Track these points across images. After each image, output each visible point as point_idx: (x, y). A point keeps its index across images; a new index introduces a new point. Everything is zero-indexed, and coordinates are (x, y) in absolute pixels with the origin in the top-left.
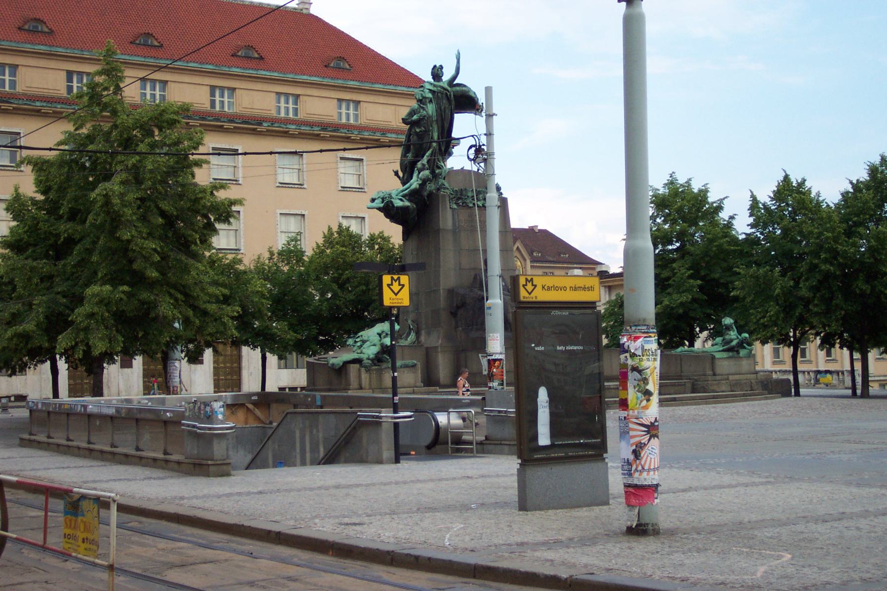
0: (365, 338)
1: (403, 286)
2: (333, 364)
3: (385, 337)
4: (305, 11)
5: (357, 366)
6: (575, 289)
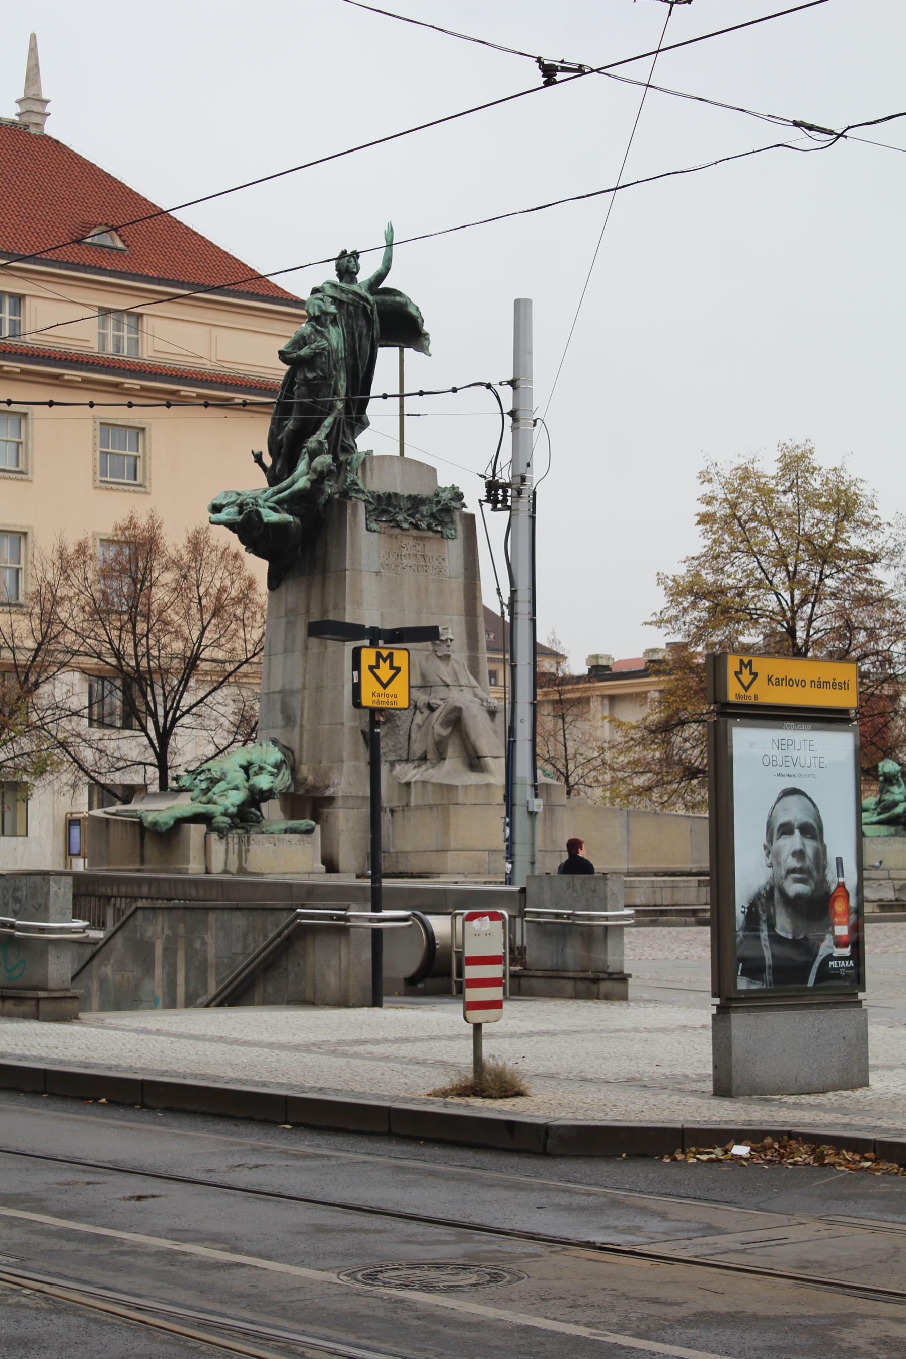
0: (216, 774)
1: (398, 670)
2: (155, 824)
3: (256, 774)
4: (33, 130)
5: (203, 828)
6: (820, 684)
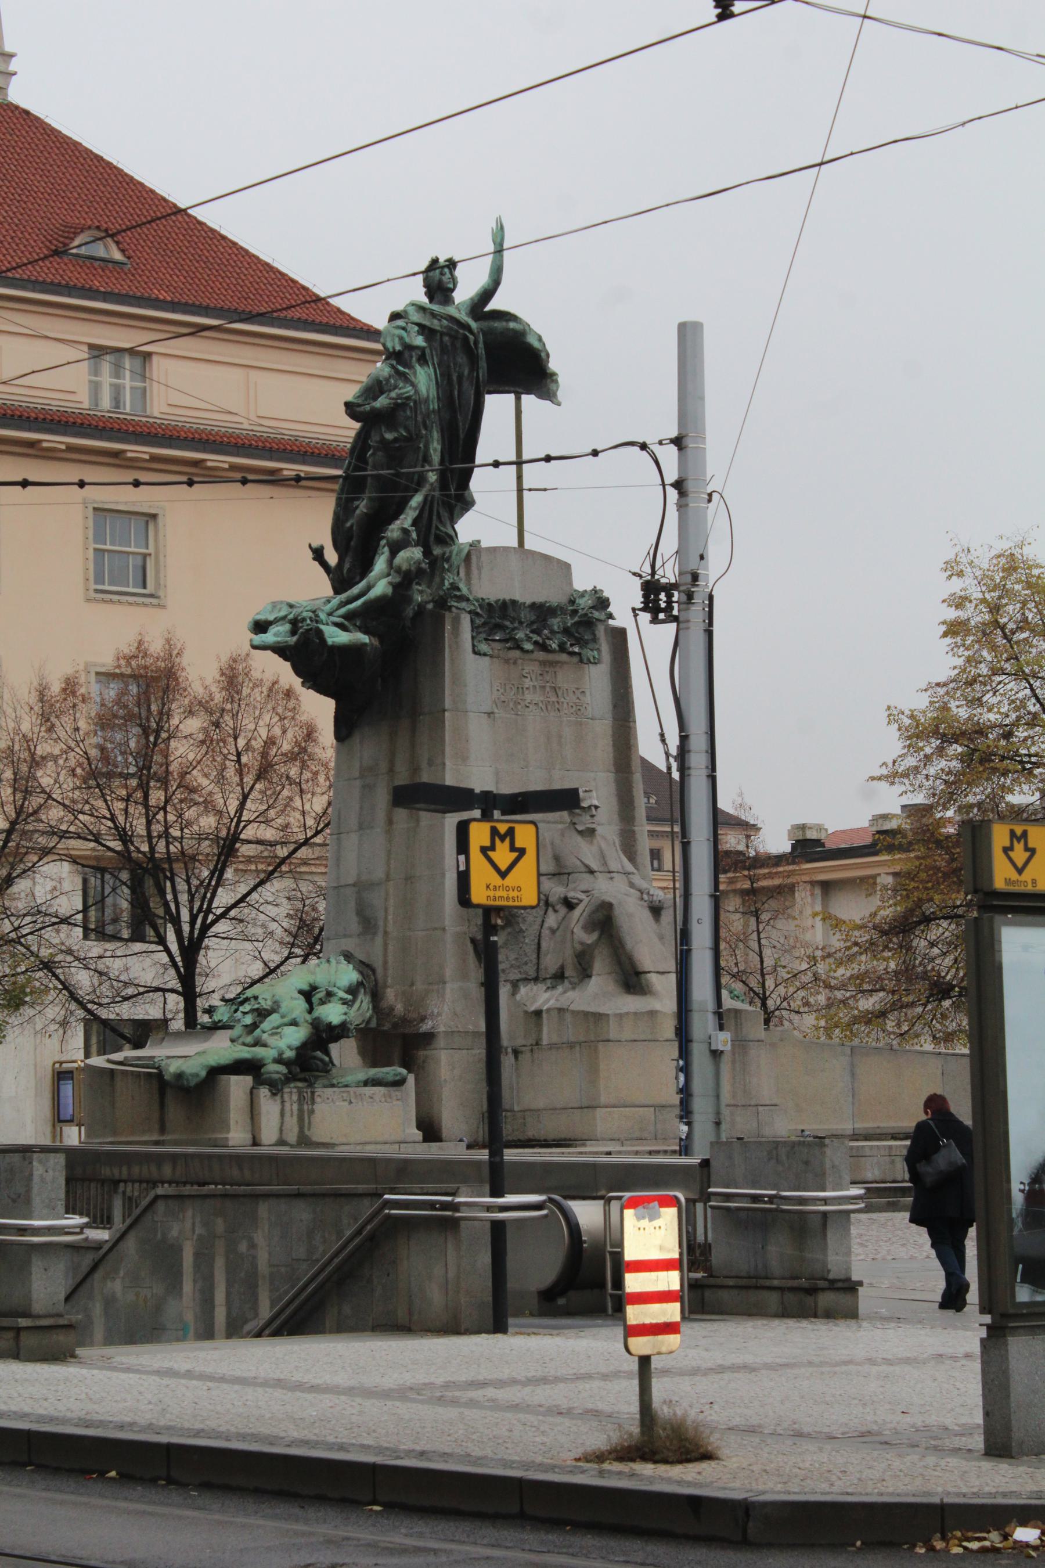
0: (266, 1005)
1: (522, 852)
2: (180, 1076)
3: (322, 1002)
5: (248, 1080)
